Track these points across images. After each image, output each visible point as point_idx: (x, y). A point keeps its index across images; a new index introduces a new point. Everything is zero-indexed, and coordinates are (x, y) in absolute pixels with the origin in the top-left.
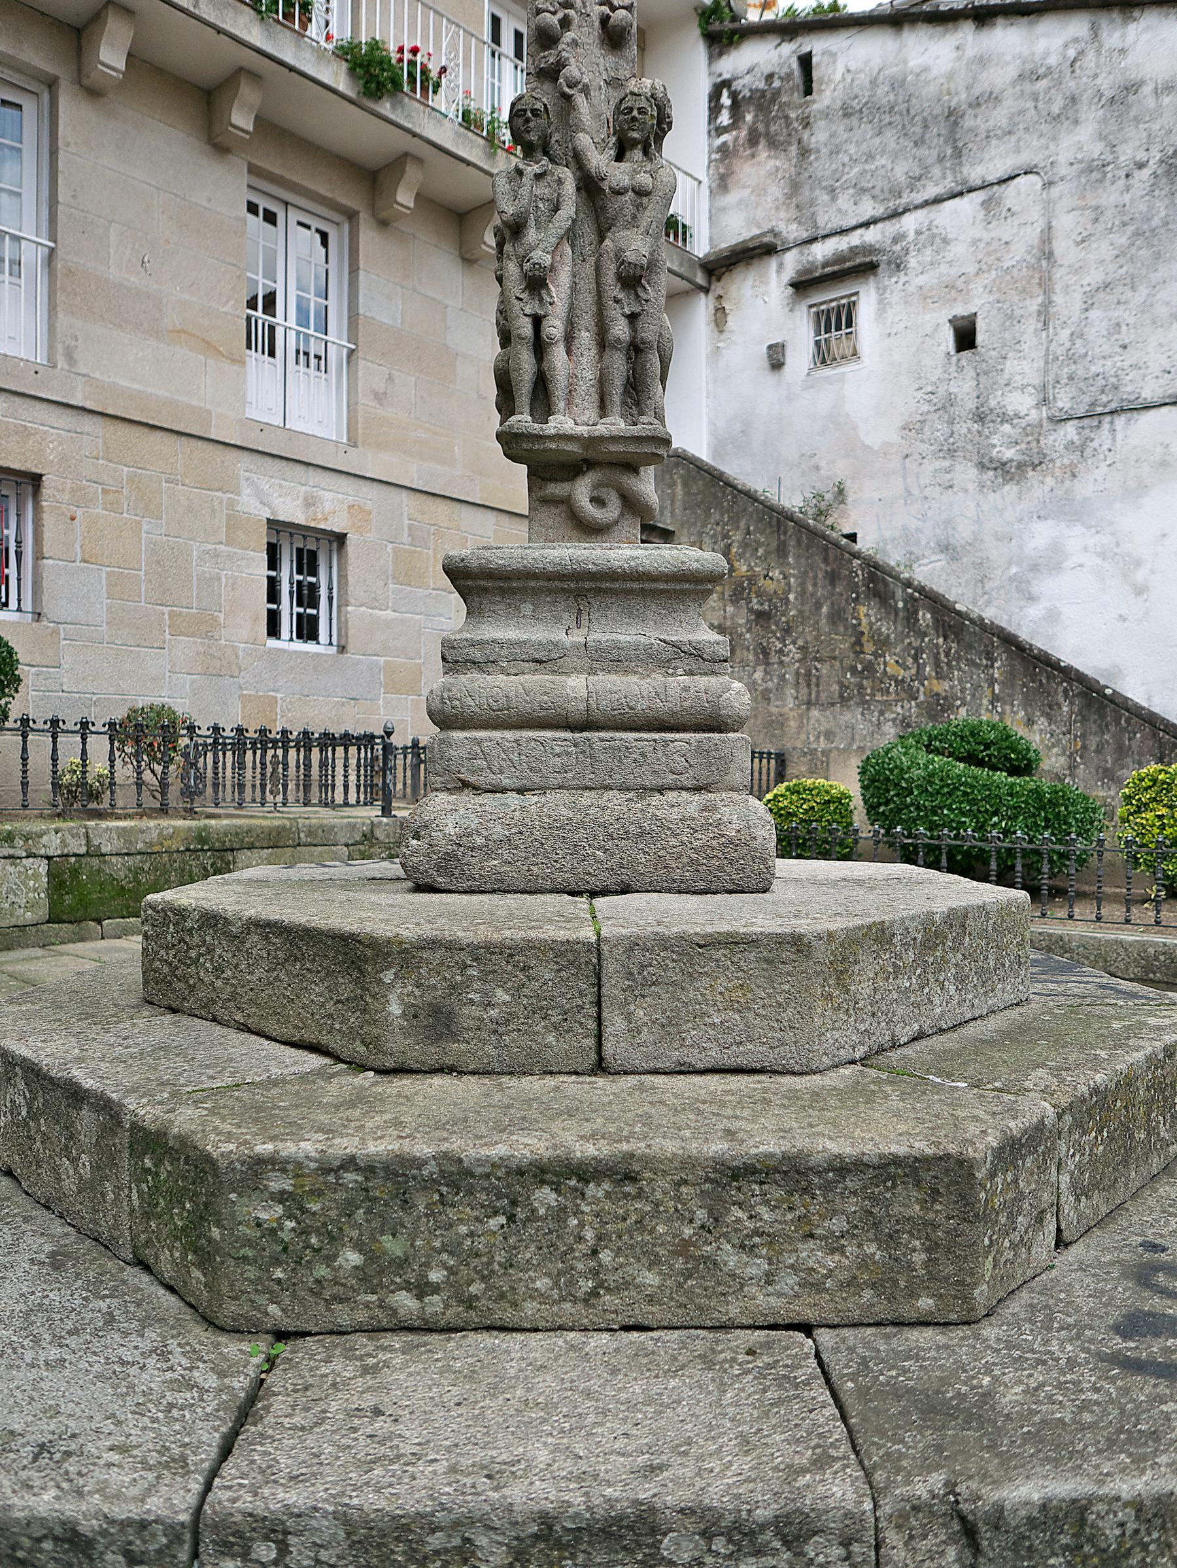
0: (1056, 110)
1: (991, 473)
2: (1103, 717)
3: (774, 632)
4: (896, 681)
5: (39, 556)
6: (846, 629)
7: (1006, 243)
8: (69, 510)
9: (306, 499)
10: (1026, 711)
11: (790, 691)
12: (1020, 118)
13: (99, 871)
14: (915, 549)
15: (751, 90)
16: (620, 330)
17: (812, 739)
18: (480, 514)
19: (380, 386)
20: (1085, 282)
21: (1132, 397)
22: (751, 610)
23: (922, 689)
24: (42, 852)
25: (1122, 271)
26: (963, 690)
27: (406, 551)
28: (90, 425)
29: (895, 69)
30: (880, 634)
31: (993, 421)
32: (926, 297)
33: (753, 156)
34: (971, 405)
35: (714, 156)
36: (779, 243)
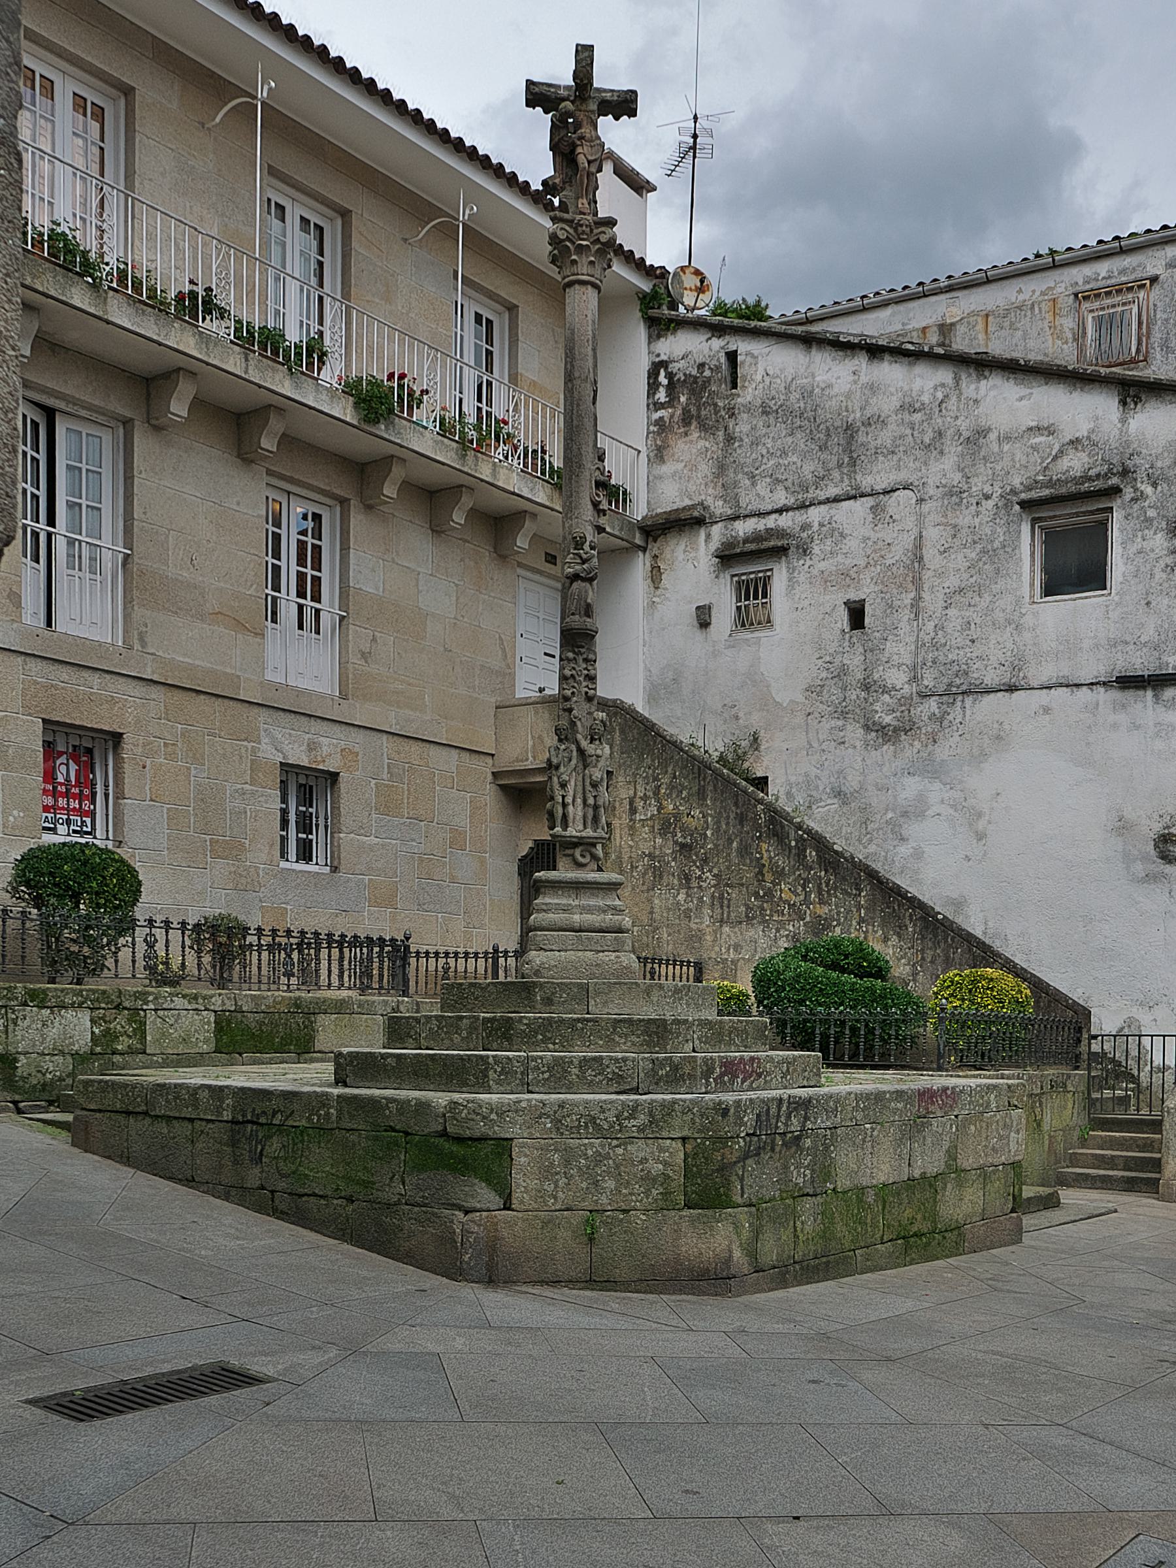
0: (927, 441)
1: (873, 734)
2: (936, 936)
3: (694, 862)
4: (789, 905)
5: (120, 795)
6: (751, 861)
7: (888, 544)
8: (141, 760)
9: (308, 745)
10: (883, 930)
11: (707, 911)
12: (901, 441)
13: (242, 1021)
14: (814, 793)
15: (685, 374)
16: (591, 801)
17: (724, 950)
18: (444, 752)
19: (366, 647)
20: (946, 585)
21: (978, 682)
22: (676, 842)
23: (808, 912)
24: (212, 1008)
25: (972, 580)
26: (838, 913)
27: (387, 786)
28: (156, 693)
29: (805, 381)
30: (778, 867)
31: (876, 691)
32: (826, 580)
33: (686, 434)
34: (860, 676)
35: (652, 428)
36: (707, 516)
